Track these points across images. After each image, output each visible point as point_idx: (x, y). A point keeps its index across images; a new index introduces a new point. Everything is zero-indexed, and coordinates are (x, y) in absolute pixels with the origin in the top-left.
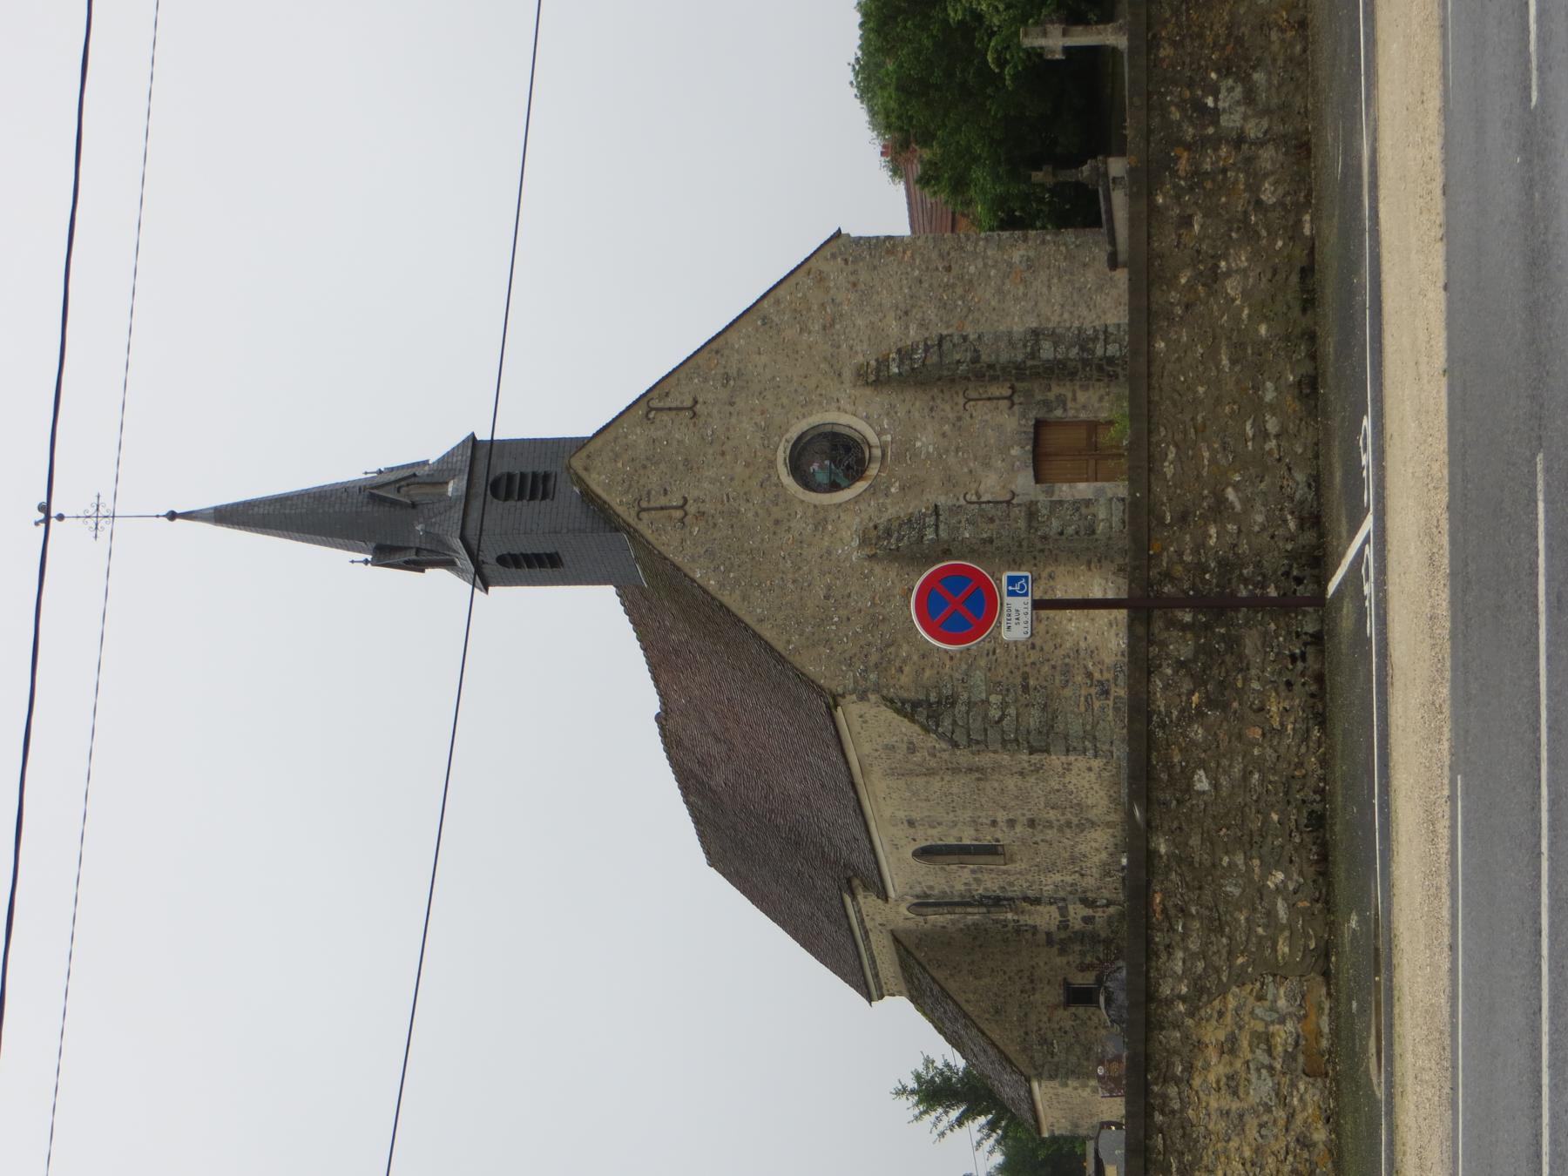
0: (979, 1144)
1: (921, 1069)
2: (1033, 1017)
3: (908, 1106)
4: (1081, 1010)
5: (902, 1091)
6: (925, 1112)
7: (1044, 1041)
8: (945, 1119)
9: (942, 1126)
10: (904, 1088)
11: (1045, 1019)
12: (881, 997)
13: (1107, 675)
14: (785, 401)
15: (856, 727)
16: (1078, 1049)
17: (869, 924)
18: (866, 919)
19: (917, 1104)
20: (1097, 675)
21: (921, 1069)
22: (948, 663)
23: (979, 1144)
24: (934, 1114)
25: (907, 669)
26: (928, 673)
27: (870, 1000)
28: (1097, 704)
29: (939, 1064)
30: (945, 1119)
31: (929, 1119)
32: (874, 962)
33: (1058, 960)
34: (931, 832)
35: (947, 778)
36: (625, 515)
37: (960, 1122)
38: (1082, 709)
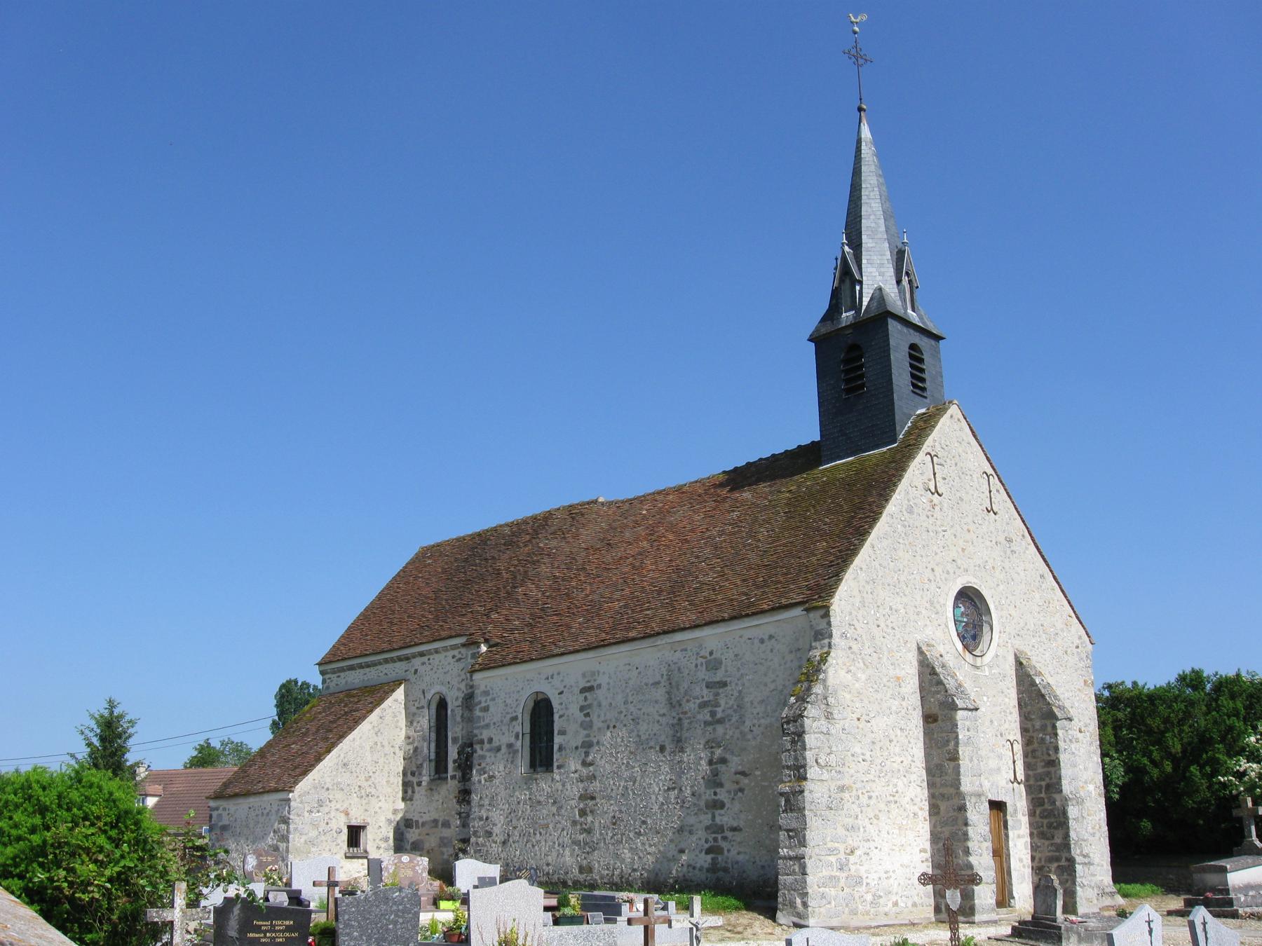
0: (72, 756)
1: (127, 718)
2: (339, 795)
3: (101, 708)
4: (344, 836)
5: (112, 705)
6: (97, 722)
7: (320, 803)
8: (92, 734)
9: (87, 732)
10: (115, 707)
11: (338, 806)
12: (322, 673)
13: (853, 868)
14: (1001, 587)
15: (748, 634)
16: (314, 833)
17: (417, 662)
18: (425, 659)
19: (102, 716)
20: (852, 859)
21: (127, 718)
22: (855, 716)
23: (72, 756)
24: (95, 727)
25: (849, 676)
26: (848, 696)
27: (319, 664)
28: (833, 859)
29: (131, 731)
30: (92, 734)
31: (93, 724)
32: (368, 666)
33: (383, 819)
34: (574, 710)
35: (663, 720)
36: (927, 443)
37: (89, 744)
38: (830, 845)
